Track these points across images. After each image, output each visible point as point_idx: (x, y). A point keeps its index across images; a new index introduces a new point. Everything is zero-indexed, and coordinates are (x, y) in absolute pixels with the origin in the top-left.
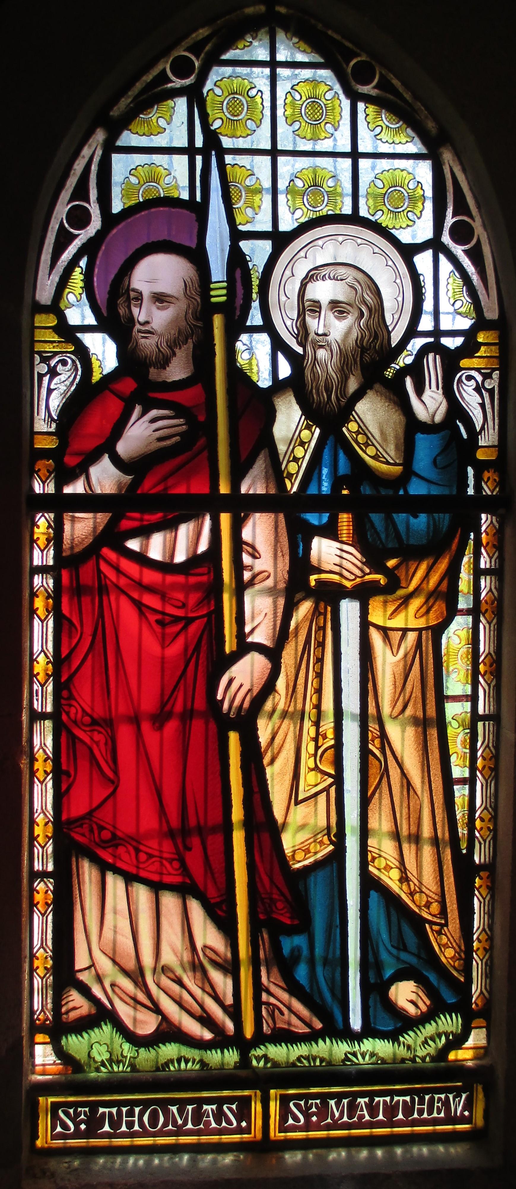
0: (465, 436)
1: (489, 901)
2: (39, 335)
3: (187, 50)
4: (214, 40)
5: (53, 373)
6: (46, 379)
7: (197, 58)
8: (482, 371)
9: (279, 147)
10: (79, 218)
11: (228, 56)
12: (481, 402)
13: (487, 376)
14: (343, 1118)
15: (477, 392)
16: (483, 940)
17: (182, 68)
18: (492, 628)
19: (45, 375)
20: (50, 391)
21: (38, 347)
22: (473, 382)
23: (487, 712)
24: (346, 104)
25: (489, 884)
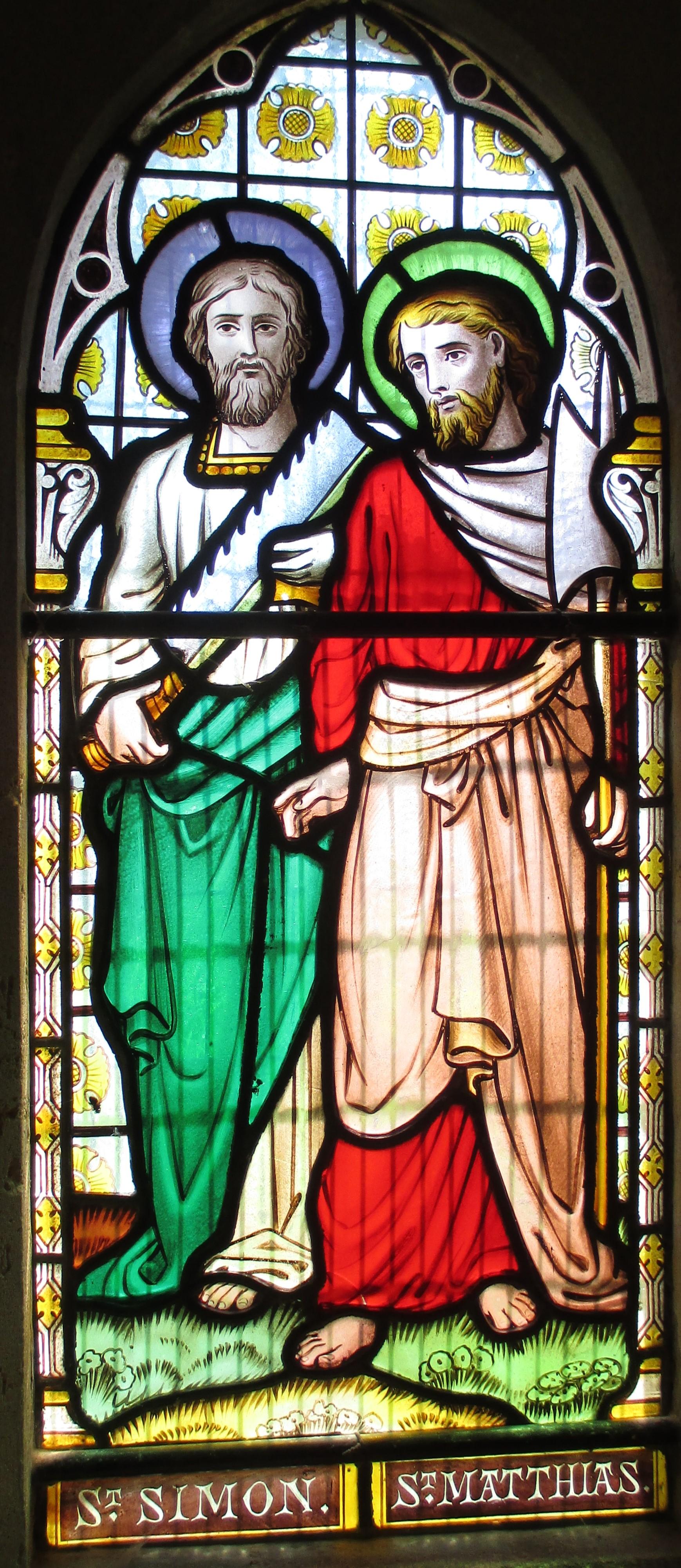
0: (608, 756)
1: (660, 1106)
2: (42, 436)
3: (244, 44)
4: (294, 21)
5: (62, 488)
6: (52, 497)
7: (256, 56)
8: (641, 469)
9: (358, 178)
10: (94, 275)
11: (296, 52)
12: (640, 511)
13: (647, 477)
14: (464, 1499)
15: (635, 499)
16: (654, 1159)
17: (234, 69)
18: (658, 896)
19: (51, 490)
20: (58, 517)
21: (41, 453)
22: (628, 487)
23: (650, 1223)
24: (449, 120)
25: (661, 1082)
